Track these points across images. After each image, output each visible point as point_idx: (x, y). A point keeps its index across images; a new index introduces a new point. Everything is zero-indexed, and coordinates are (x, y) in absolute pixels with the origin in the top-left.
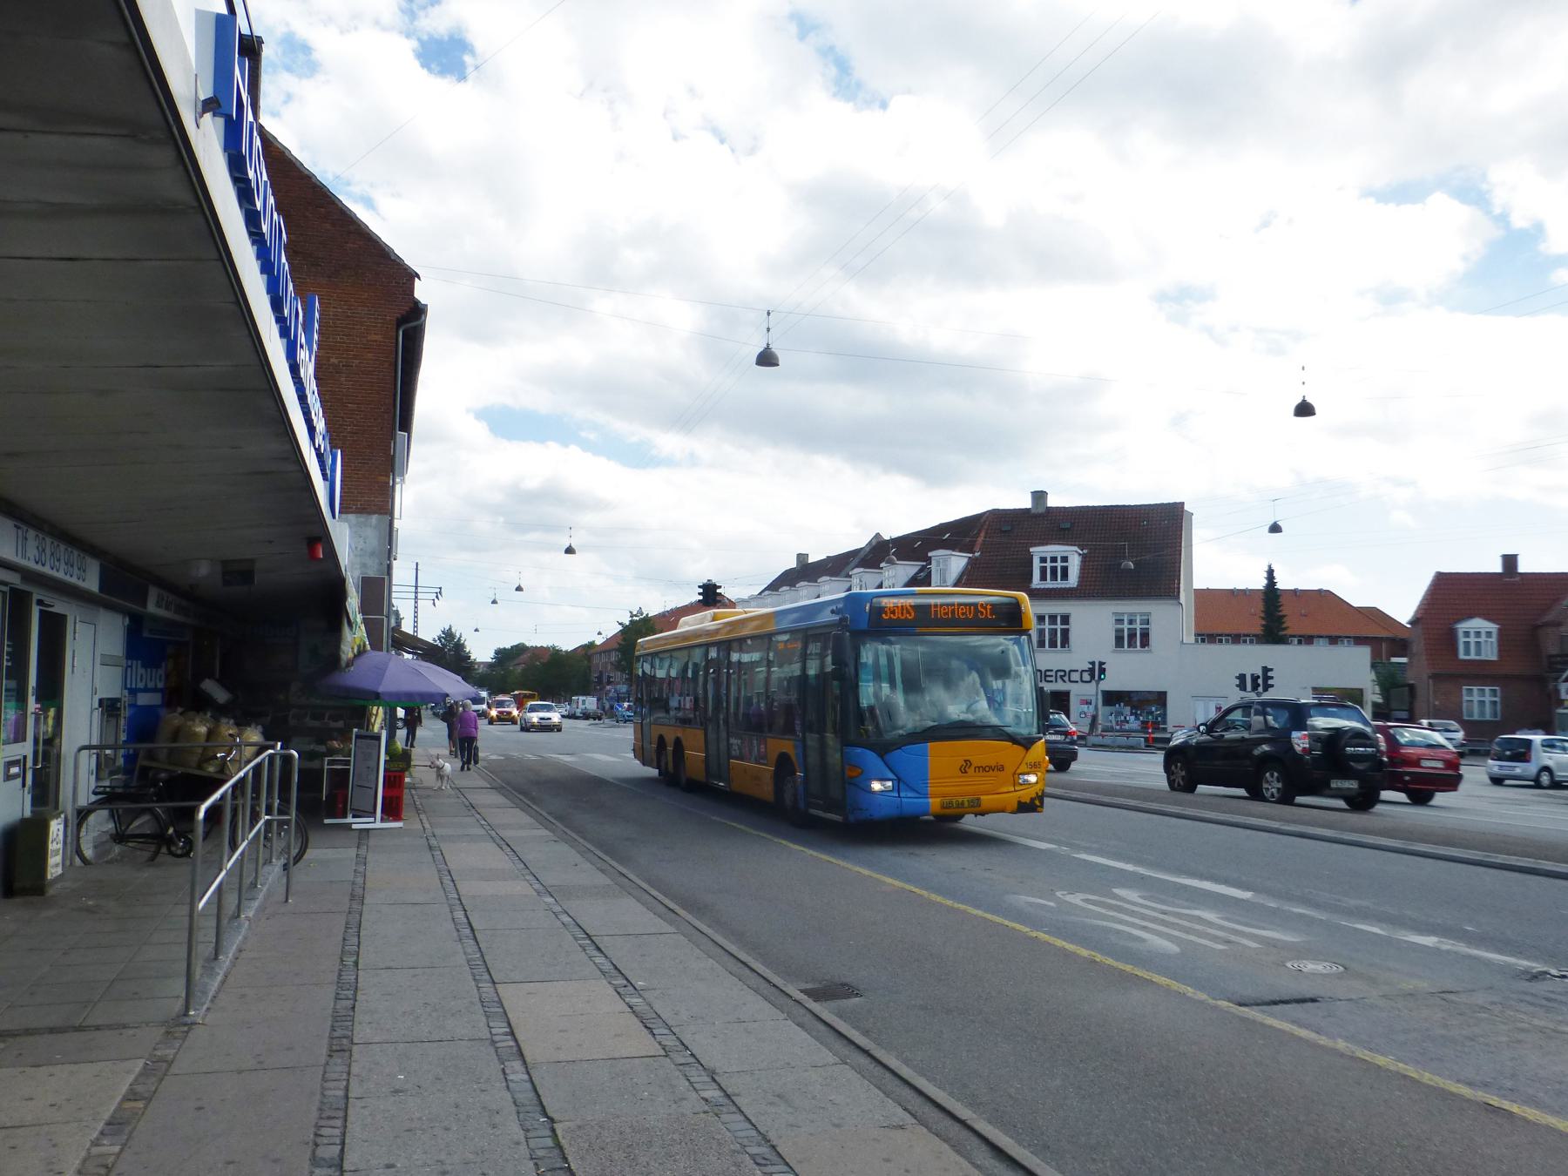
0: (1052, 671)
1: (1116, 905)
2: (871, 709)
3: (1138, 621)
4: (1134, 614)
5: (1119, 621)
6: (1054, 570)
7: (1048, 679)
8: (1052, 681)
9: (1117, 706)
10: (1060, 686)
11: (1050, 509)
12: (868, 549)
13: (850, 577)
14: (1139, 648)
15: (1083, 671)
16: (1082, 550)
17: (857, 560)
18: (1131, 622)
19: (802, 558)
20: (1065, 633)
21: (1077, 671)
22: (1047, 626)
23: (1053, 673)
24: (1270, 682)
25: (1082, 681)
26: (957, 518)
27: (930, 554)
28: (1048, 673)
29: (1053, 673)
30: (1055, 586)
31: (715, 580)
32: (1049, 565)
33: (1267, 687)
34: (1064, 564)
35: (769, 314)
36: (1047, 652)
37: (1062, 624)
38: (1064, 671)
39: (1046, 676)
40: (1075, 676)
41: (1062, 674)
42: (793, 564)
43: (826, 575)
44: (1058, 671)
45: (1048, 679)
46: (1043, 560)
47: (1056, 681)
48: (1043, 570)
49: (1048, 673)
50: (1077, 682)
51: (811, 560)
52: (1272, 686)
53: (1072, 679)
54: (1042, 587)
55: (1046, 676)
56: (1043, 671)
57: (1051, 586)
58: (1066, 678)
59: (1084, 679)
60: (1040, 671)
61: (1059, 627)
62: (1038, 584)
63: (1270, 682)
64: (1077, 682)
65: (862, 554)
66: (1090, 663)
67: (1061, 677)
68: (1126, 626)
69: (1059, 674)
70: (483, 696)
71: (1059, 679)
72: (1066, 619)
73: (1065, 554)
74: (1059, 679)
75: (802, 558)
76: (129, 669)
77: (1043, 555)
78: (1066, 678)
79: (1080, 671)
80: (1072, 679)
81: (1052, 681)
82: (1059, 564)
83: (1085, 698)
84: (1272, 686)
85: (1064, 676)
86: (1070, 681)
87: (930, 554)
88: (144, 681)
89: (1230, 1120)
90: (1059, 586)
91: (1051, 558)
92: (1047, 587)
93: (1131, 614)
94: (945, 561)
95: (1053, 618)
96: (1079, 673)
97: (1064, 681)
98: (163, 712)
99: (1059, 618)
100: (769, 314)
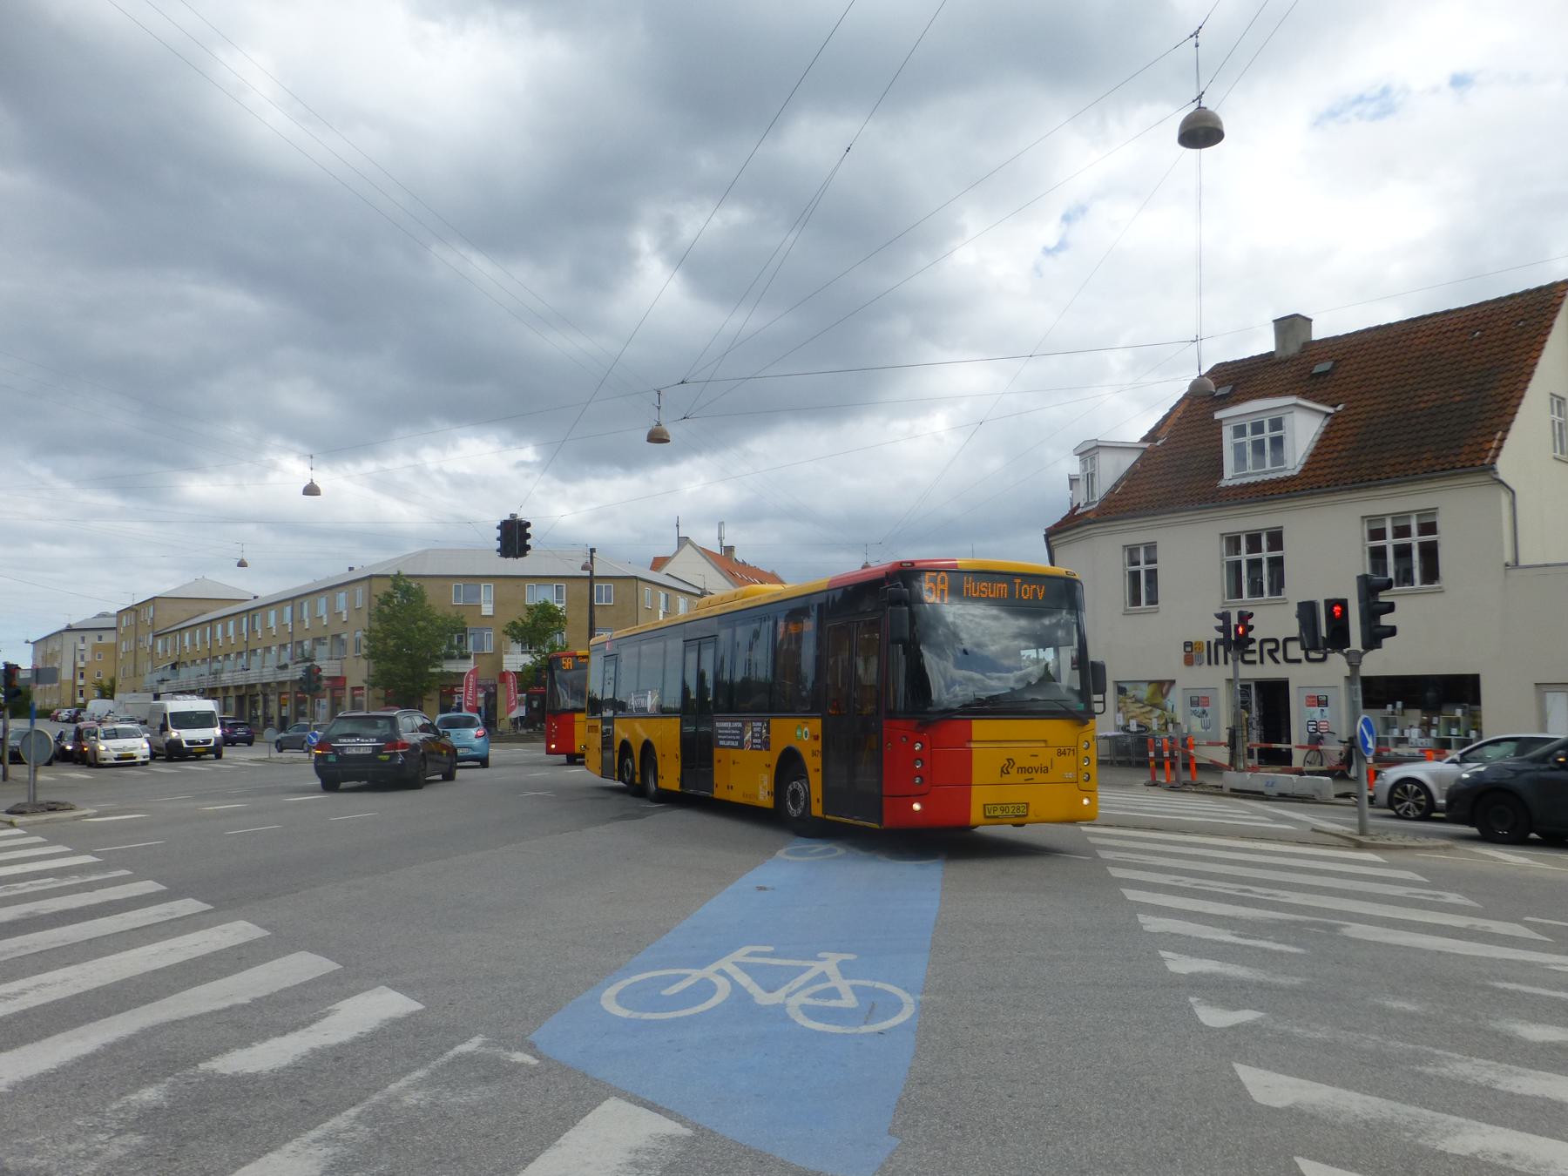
1: (89, 874)
2: (1444, 753)
3: (1414, 529)
4: (1406, 515)
5: (1378, 534)
7: (1248, 657)
8: (1254, 662)
9: (1390, 707)
14: (1417, 584)
15: (1286, 640)
16: (1334, 406)
18: (1402, 531)
20: (1277, 564)
24: (1386, 620)
31: (523, 516)
33: (1376, 636)
34: (1277, 433)
37: (1249, 552)
38: (1275, 641)
41: (1272, 646)
44: (1263, 641)
46: (1240, 431)
47: (1262, 662)
48: (1239, 449)
50: (1299, 661)
51: (1318, 333)
52: (1392, 631)
53: (1290, 656)
58: (1279, 655)
61: (1265, 555)
62: (1234, 478)
63: (1386, 620)
64: (1299, 661)
66: (1219, 616)
67: (1271, 652)
68: (1390, 542)
70: (572, 701)
71: (1266, 656)
72: (1276, 540)
73: (1275, 415)
74: (1266, 656)
76: (1043, 745)
77: (1239, 422)
78: (1279, 655)
80: (1290, 656)
81: (1254, 662)
82: (1267, 435)
83: (1316, 693)
84: (1392, 631)
85: (1276, 650)
86: (1287, 660)
89: (15, 1141)
91: (1272, 422)
93: (1396, 517)
95: (1254, 542)
97: (1277, 661)
98: (33, 685)
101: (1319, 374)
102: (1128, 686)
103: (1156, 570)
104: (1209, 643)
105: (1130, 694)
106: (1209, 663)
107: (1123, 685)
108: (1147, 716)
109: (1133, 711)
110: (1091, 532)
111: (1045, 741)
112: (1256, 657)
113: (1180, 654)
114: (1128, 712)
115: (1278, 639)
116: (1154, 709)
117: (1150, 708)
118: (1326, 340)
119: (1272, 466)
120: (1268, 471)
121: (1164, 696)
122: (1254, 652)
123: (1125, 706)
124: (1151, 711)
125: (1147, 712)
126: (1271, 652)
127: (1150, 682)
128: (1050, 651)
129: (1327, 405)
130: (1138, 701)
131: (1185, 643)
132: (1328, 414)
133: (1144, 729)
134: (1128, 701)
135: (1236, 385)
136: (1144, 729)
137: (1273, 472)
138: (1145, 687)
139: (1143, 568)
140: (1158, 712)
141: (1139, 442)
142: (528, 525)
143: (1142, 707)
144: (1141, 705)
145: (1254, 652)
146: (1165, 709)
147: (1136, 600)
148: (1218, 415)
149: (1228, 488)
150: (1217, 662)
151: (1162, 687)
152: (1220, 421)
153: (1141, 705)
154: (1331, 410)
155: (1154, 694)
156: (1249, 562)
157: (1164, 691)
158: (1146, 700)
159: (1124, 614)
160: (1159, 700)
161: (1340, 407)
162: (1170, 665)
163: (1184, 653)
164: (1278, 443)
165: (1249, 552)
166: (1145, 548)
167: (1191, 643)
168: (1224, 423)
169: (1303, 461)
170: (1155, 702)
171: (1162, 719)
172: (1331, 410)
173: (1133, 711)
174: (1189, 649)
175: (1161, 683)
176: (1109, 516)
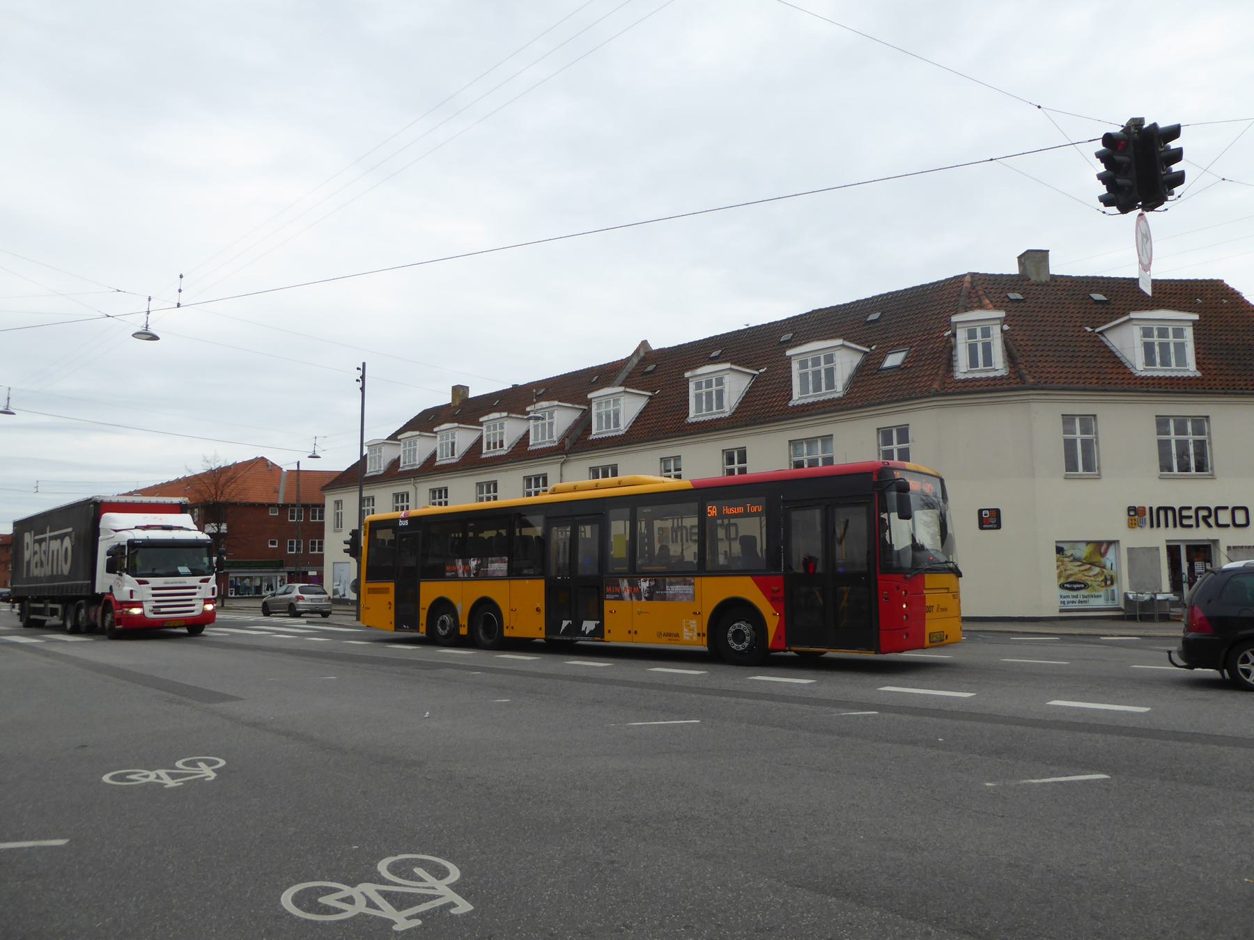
0: (1189, 508)
6: (1164, 347)
7: (1185, 522)
8: (1191, 526)
10: (1202, 534)
11: (1054, 277)
12: (635, 361)
13: (400, 440)
14: (1193, 471)
15: (1217, 509)
16: (869, 347)
17: (622, 376)
19: (459, 391)
20: (1201, 447)
21: (1226, 508)
22: (492, 494)
23: (1192, 513)
25: (1236, 525)
26: (578, 369)
27: (590, 396)
28: (1185, 513)
29: (1192, 513)
30: (1168, 374)
32: (1156, 340)
35: (150, 299)
36: (1081, 478)
38: (1208, 509)
39: (1182, 517)
40: (1224, 517)
41: (1205, 513)
42: (446, 399)
43: (495, 412)
44: (1198, 509)
45: (1185, 522)
46: (803, 365)
47: (1198, 525)
49: (1185, 513)
50: (1228, 526)
51: (471, 395)
54: (1149, 374)
55: (1182, 517)
56: (689, 527)
57: (1161, 374)
59: (1238, 522)
60: (1173, 509)
65: (630, 366)
67: (1205, 519)
69: (1202, 513)
71: (1201, 523)
72: (904, 434)
74: (1201, 523)
75: (459, 391)
77: (802, 358)
79: (1230, 508)
80: (1220, 522)
81: (1191, 526)
85: (1210, 516)
86: (1218, 525)
87: (590, 396)
88: (64, 549)
90: (1174, 374)
92: (1155, 374)
94: (616, 401)
96: (1229, 512)
97: (1209, 526)
99: (1189, 425)
100: (150, 299)
101: (872, 321)
102: (1065, 546)
103: (832, 457)
104: (1151, 509)
105: (1068, 553)
106: (1152, 526)
107: (1061, 545)
108: (1086, 573)
109: (1071, 569)
110: (1031, 397)
111: (948, 589)
112: (1192, 522)
113: (1123, 517)
114: (1066, 570)
115: (1175, 507)
116: (1093, 567)
117: (1089, 566)
118: (474, 398)
119: (984, 366)
120: (715, 414)
121: (1103, 555)
122: (1190, 517)
123: (1062, 565)
124: (1089, 569)
125: (1086, 570)
126: (1205, 519)
127: (1088, 543)
128: (886, 514)
129: (864, 346)
130: (1075, 560)
131: (1129, 507)
132: (866, 353)
133: (1083, 586)
134: (1066, 559)
135: (882, 313)
136: (1083, 586)
137: (706, 415)
138: (1083, 546)
139: (1078, 436)
140: (1097, 570)
141: (386, 439)
142: (1174, 132)
143: (1080, 566)
144: (1080, 563)
145: (1190, 517)
146: (1104, 567)
147: (1071, 465)
148: (789, 353)
149: (693, 424)
150: (1159, 525)
151: (1101, 547)
152: (790, 357)
153: (1080, 563)
154: (867, 350)
155: (1091, 554)
156: (899, 450)
157: (1103, 550)
158: (1085, 559)
159: (1065, 478)
160: (1096, 559)
161: (873, 348)
162: (1114, 527)
163: (1127, 517)
164: (720, 394)
165: (899, 443)
166: (897, 430)
167: (1135, 507)
168: (793, 358)
169: (735, 407)
170: (1093, 560)
171: (1101, 576)
172: (867, 350)
173: (1071, 569)
174: (1132, 513)
175: (1099, 544)
176: (823, 410)
